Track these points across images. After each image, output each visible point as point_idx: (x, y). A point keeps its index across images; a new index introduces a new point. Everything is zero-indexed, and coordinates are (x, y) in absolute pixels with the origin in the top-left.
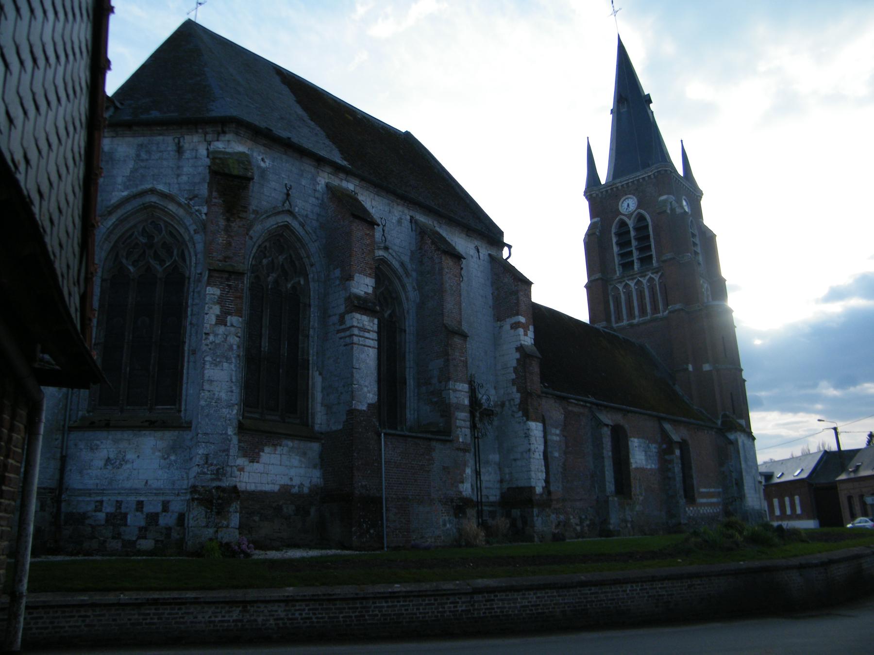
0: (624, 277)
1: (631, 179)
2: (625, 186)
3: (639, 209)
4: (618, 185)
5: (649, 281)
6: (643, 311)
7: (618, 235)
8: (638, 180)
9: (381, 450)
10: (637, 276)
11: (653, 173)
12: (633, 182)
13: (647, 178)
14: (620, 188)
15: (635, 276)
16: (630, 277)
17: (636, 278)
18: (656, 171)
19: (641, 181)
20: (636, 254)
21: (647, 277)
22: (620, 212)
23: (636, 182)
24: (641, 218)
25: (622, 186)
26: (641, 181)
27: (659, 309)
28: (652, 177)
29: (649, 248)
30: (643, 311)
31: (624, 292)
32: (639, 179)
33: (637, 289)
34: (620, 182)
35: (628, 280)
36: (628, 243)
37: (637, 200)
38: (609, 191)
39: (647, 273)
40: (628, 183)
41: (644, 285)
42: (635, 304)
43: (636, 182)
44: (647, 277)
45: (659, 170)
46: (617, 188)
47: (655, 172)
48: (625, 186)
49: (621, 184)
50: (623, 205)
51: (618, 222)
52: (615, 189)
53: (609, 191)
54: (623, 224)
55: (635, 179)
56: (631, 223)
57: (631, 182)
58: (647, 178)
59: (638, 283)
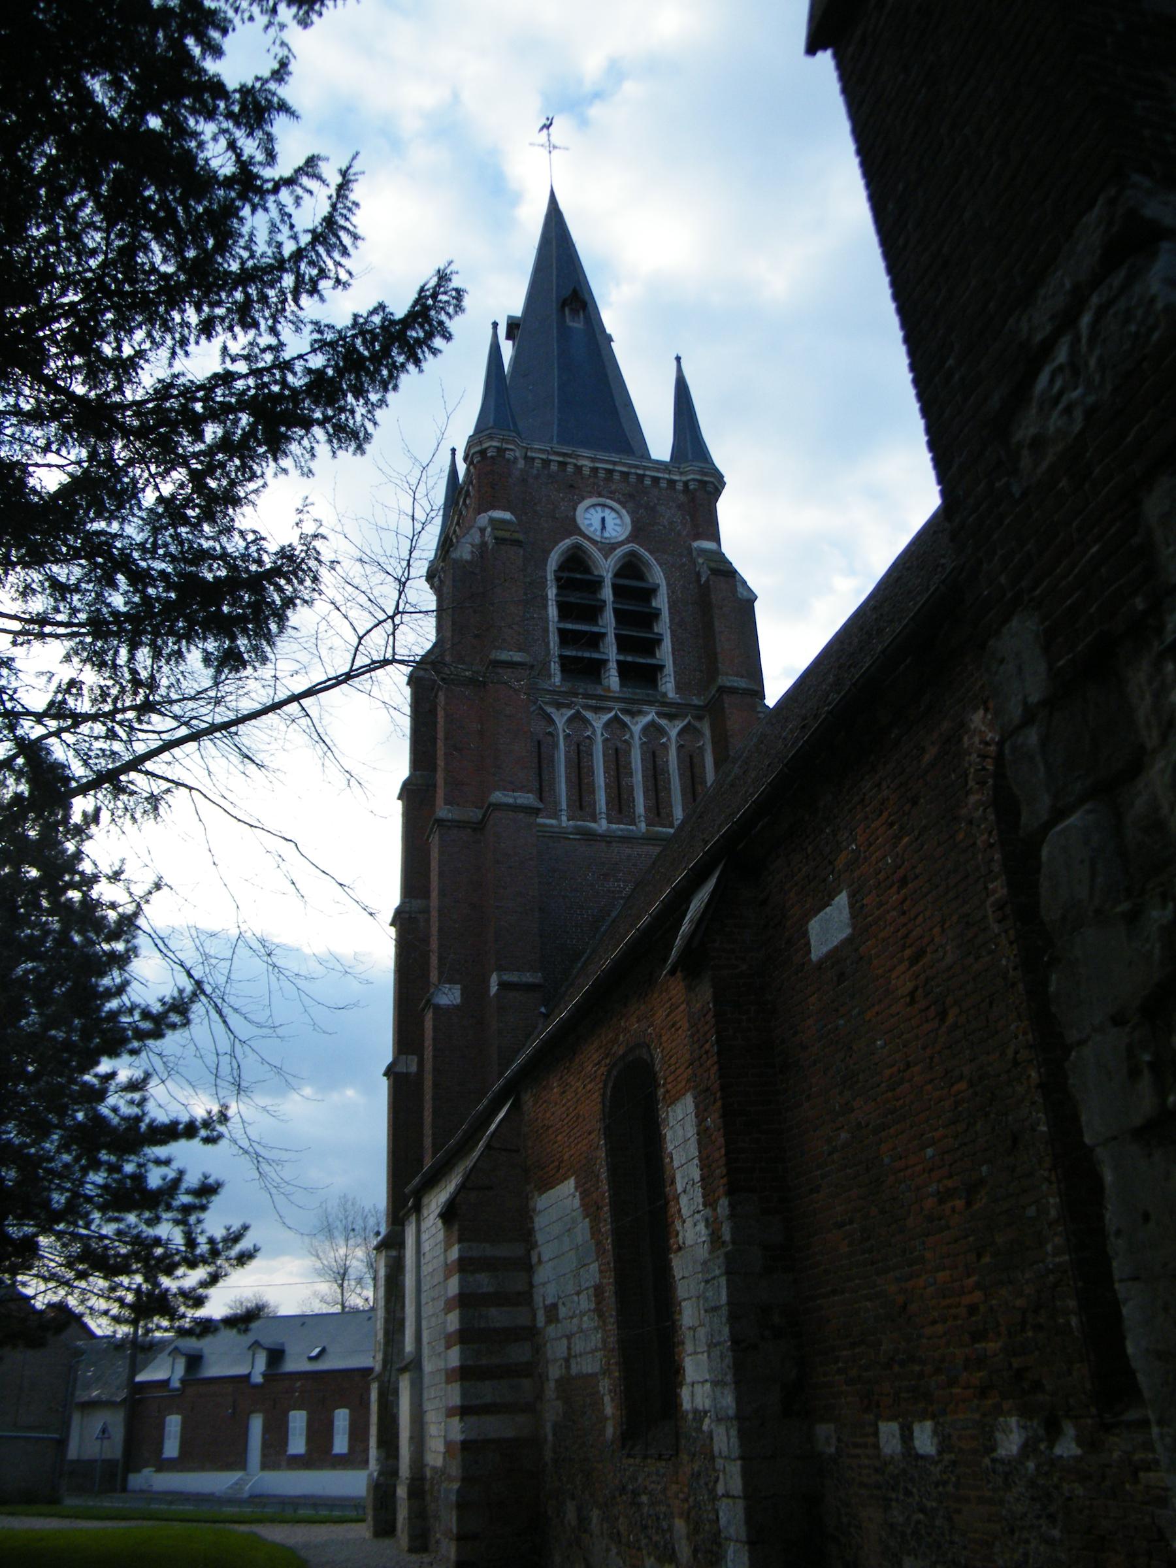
0: (576, 695)
1: (624, 464)
2: (602, 474)
3: (633, 542)
4: (581, 462)
5: (646, 730)
6: (620, 804)
7: (564, 585)
8: (641, 478)
9: (162, 1396)
10: (617, 705)
11: (684, 478)
12: (625, 475)
13: (663, 484)
14: (586, 472)
15: (610, 704)
16: (592, 702)
17: (610, 709)
18: (698, 477)
19: (648, 482)
20: (611, 651)
21: (645, 720)
22: (580, 529)
23: (632, 479)
24: (631, 568)
25: (595, 470)
26: (648, 482)
27: (593, 804)
28: (680, 487)
29: (652, 645)
30: (620, 804)
31: (567, 736)
32: (644, 476)
33: (644, 743)
34: (593, 460)
35: (587, 707)
36: (593, 612)
37: (632, 521)
38: (554, 467)
39: (646, 708)
40: (610, 472)
41: (632, 737)
42: (600, 779)
43: (632, 479)
44: (645, 720)
45: (706, 479)
46: (578, 469)
47: (694, 480)
48: (602, 474)
49: (592, 465)
50: (592, 511)
51: (569, 549)
52: (570, 469)
53: (554, 467)
54: (576, 561)
55: (633, 471)
56: (606, 568)
57: (621, 472)
58: (663, 484)
59: (577, 719)
